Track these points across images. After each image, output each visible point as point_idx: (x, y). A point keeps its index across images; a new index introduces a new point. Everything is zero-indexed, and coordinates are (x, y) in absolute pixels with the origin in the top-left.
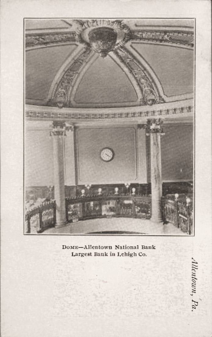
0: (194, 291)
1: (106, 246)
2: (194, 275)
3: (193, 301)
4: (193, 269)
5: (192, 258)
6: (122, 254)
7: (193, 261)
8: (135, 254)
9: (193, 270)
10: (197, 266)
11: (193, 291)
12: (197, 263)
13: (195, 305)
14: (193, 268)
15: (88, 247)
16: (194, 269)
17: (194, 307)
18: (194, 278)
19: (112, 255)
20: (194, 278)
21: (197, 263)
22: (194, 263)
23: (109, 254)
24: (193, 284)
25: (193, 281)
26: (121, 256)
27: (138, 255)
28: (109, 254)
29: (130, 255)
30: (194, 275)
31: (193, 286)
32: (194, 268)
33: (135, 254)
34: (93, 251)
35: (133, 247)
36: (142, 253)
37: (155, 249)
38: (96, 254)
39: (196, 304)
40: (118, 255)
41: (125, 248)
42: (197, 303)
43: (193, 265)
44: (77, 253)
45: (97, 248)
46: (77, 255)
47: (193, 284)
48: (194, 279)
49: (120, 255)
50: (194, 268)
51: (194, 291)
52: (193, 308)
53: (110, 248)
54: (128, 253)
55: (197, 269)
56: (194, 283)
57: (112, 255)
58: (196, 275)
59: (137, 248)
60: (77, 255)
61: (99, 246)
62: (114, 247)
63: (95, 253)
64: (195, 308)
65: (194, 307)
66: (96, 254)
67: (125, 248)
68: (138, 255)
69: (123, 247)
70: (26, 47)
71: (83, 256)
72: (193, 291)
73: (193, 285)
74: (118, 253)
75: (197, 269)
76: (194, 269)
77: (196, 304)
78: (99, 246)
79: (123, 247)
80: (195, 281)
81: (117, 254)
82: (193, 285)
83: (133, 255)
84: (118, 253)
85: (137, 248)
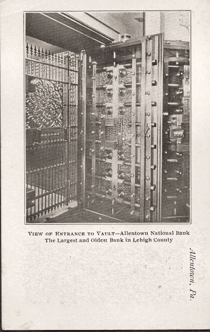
0: (192, 281)
1: (50, 232)
2: (192, 264)
3: (191, 290)
4: (191, 259)
5: (190, 249)
6: (137, 240)
7: (191, 252)
8: (150, 240)
9: (191, 260)
10: (195, 257)
11: (192, 281)
12: (195, 253)
13: (192, 294)
14: (191, 258)
15: (124, 233)
16: (192, 259)
17: (192, 296)
18: (192, 268)
19: (127, 240)
20: (192, 268)
21: (195, 253)
22: (192, 253)
23: (124, 240)
24: (191, 274)
25: (191, 270)
26: (137, 242)
27: (152, 240)
28: (124, 240)
29: (145, 241)
30: (192, 264)
31: (191, 275)
32: (192, 258)
33: (150, 240)
34: (131, 237)
35: (81, 235)
36: (158, 239)
37: (189, 234)
38: (112, 240)
39: (194, 293)
40: (133, 240)
41: (160, 234)
42: (195, 292)
43: (191, 255)
44: (81, 239)
45: (134, 234)
46: (62, 241)
47: (191, 274)
48: (192, 269)
49: (135, 241)
50: (192, 258)
51: (192, 281)
52: (191, 297)
53: (146, 234)
54: (143, 239)
55: (195, 259)
56: (192, 273)
57: (127, 240)
58: (190, 269)
59: (172, 233)
60: (62, 241)
61: (136, 232)
62: (149, 233)
63: (111, 239)
64: (193, 297)
65: (193, 296)
66: (112, 240)
67: (160, 234)
68: (152, 240)
69: (158, 233)
70: (26, 14)
71: (147, 242)
72: (192, 281)
73: (191, 274)
74: (134, 239)
75: (195, 259)
76: (192, 259)
77: (194, 293)
78: (136, 232)
79: (158, 233)
80: (192, 271)
81: (132, 240)
82: (191, 274)
83: (148, 241)
84: (134, 239)
85: (172, 233)
